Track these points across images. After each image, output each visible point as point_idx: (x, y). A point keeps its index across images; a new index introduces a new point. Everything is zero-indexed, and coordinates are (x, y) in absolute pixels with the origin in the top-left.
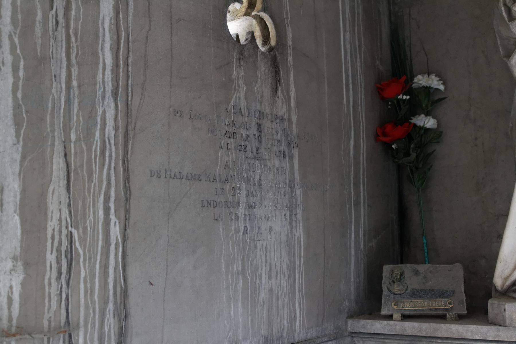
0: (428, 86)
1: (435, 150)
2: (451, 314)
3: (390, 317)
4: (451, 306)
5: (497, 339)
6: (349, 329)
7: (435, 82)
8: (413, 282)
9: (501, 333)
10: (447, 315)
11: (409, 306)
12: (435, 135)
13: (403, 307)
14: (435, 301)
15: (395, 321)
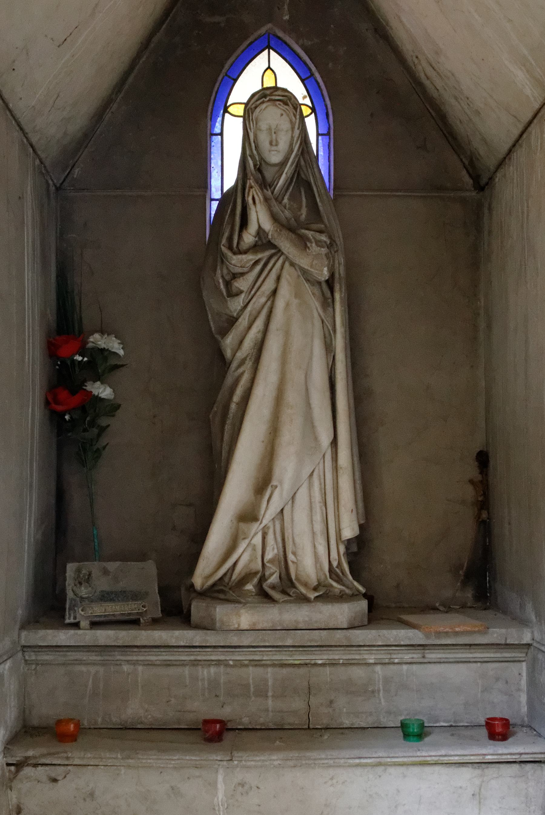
0: (106, 348)
1: (109, 425)
2: (145, 618)
3: (76, 626)
4: (145, 609)
5: (204, 645)
6: (23, 642)
7: (114, 345)
8: (102, 584)
9: (208, 638)
10: (141, 619)
11: (100, 610)
12: (113, 408)
13: (91, 613)
14: (128, 605)
15: (82, 629)
